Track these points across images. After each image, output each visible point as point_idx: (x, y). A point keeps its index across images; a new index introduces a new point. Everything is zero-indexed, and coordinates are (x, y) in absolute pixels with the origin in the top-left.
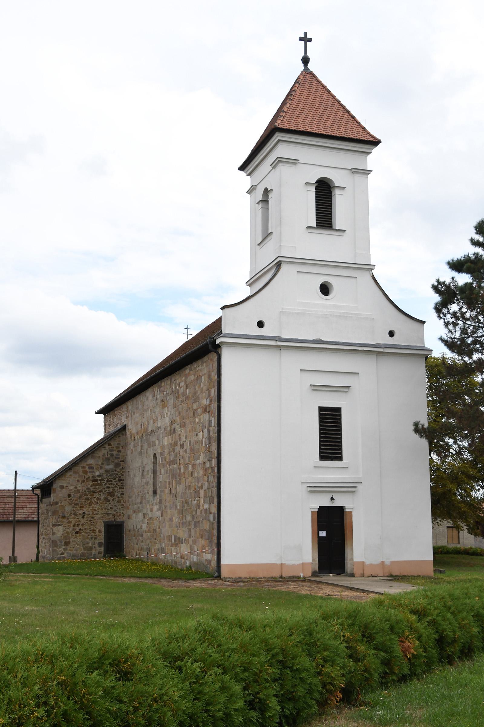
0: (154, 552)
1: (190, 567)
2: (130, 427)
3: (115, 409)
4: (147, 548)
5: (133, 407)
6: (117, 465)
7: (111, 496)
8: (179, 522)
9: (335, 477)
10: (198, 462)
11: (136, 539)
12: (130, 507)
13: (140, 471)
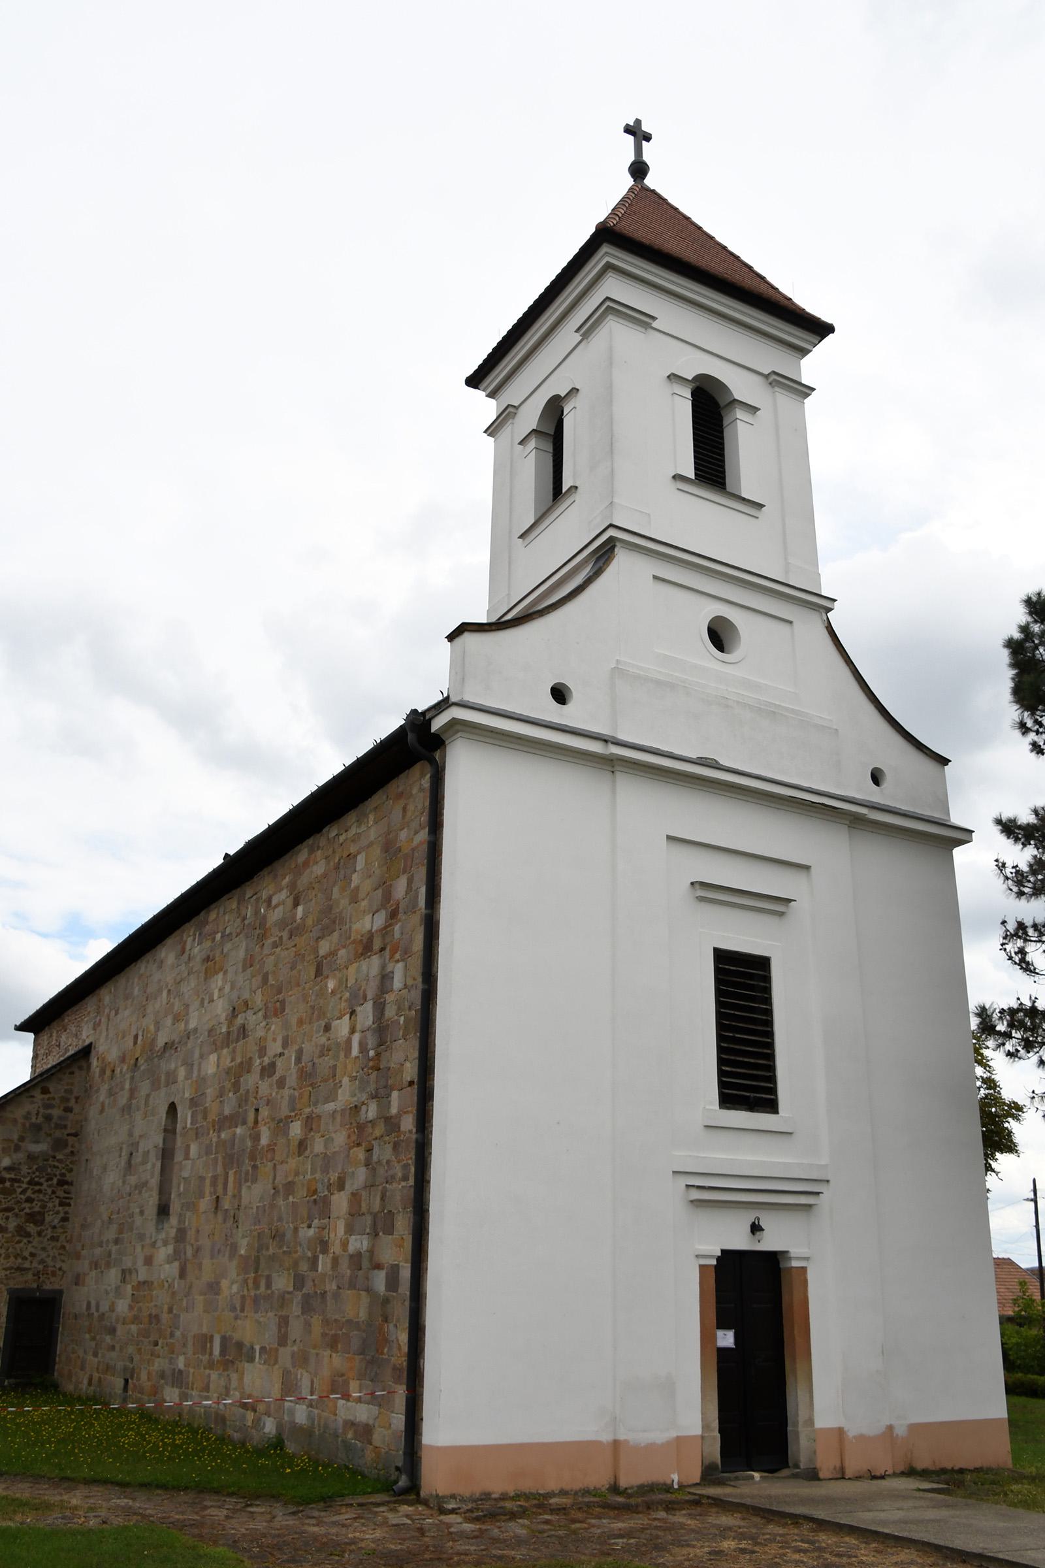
0: (149, 1379)
1: (278, 1443)
2: (101, 1047)
3: (66, 1014)
4: (125, 1369)
5: (115, 996)
6: (59, 1144)
7: (36, 1223)
8: (243, 1297)
9: (773, 1160)
10: (331, 1106)
11: (93, 1339)
12: (84, 1252)
13: (120, 1156)
